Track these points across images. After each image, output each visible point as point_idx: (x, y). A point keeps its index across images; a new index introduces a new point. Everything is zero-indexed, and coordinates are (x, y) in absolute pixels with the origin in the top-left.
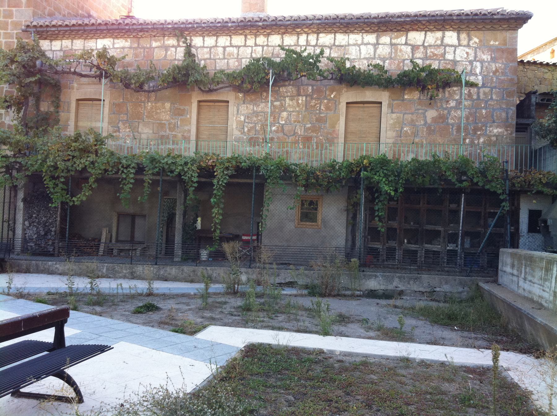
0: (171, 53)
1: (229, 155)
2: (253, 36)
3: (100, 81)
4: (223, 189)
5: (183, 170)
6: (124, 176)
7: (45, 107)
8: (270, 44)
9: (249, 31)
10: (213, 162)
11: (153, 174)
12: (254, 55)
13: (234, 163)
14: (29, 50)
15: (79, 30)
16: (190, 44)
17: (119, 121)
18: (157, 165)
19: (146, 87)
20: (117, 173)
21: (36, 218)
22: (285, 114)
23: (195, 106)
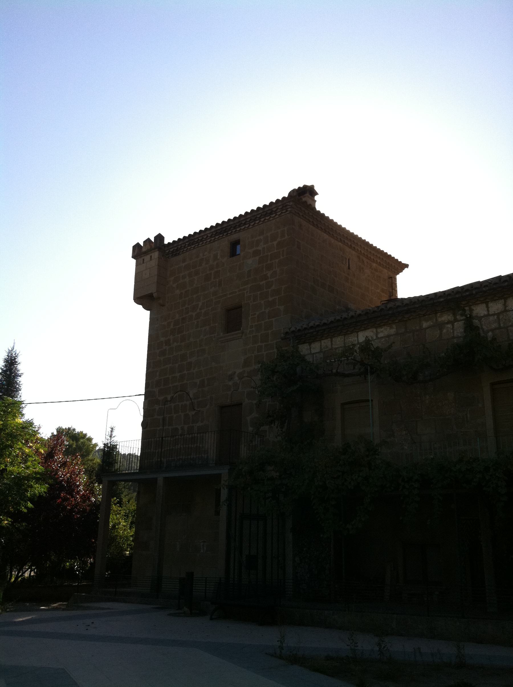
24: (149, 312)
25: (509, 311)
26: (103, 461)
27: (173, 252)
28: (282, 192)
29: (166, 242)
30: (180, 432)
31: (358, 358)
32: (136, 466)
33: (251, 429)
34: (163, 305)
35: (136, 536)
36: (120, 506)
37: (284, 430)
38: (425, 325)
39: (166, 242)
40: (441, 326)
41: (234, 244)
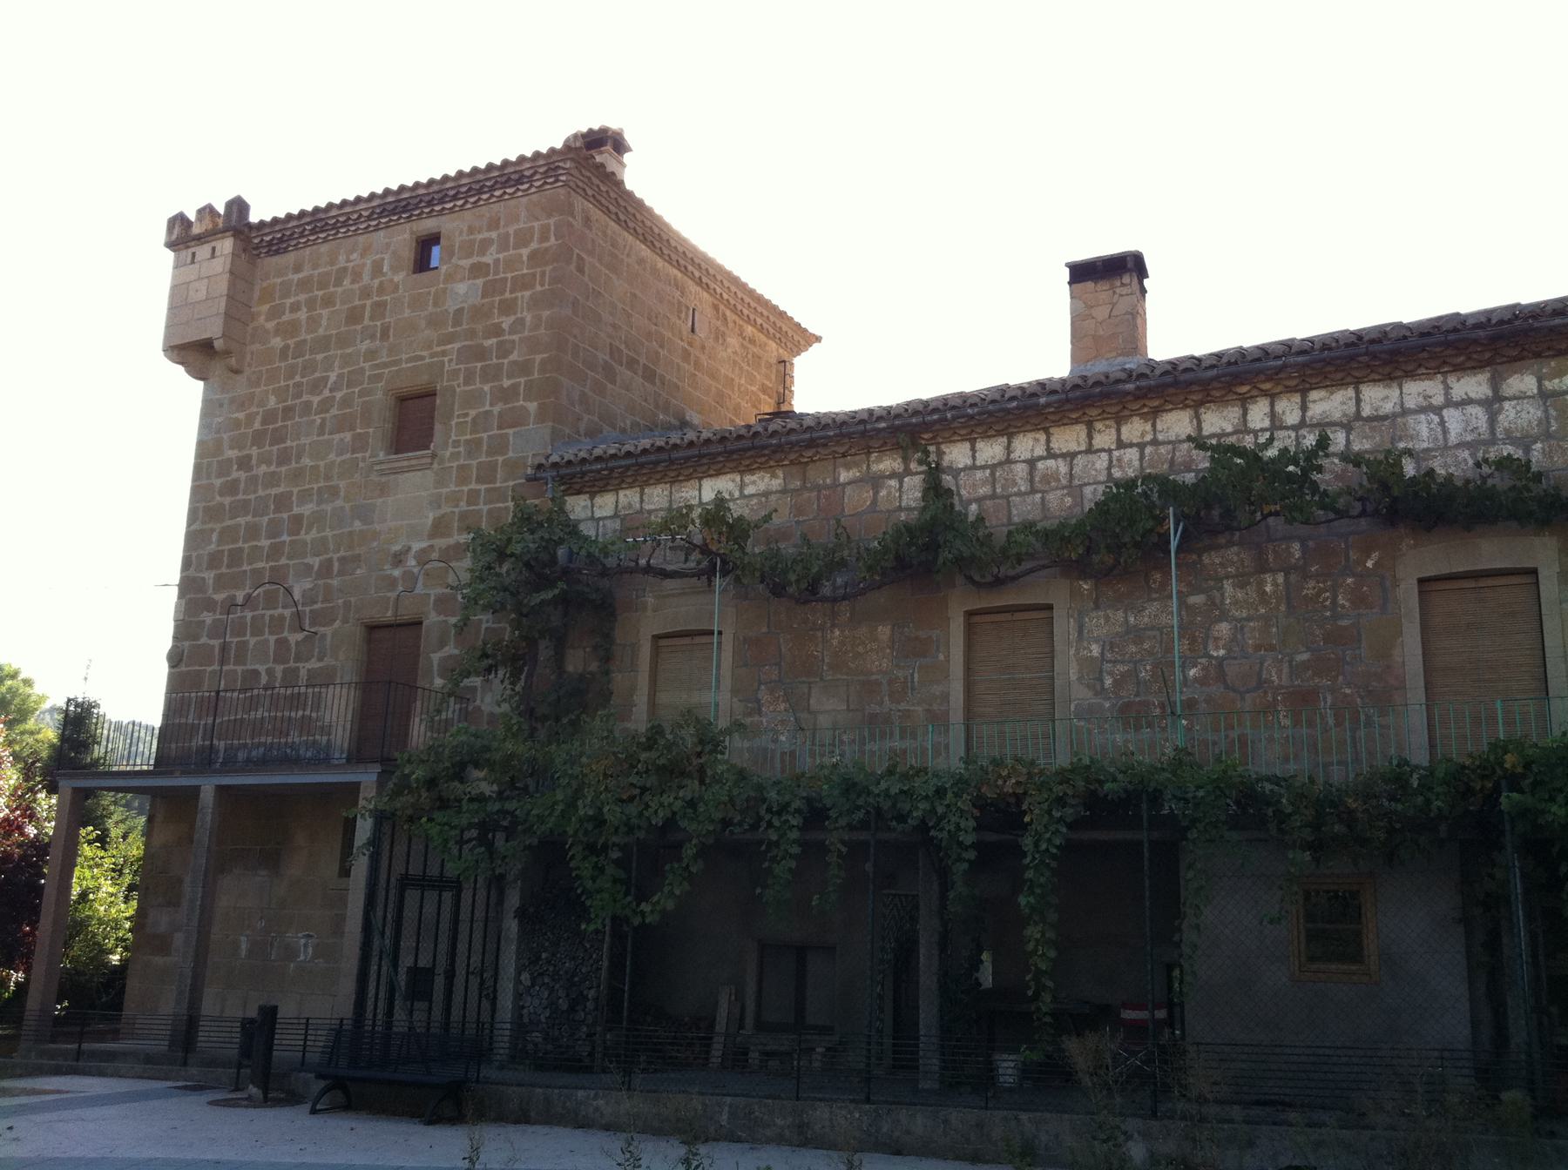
0: (889, 493)
1: (1063, 760)
2: (1111, 423)
4: (1054, 864)
5: (933, 811)
7: (576, 661)
8: (1160, 437)
10: (1018, 783)
11: (851, 827)
12: (1117, 473)
14: (540, 525)
18: (860, 802)
19: (826, 589)
21: (549, 962)
22: (1224, 628)
24: (201, 384)
26: (63, 738)
27: (270, 243)
28: (550, 136)
29: (254, 218)
30: (264, 679)
31: (697, 540)
32: (146, 754)
33: (439, 682)
34: (237, 372)
35: (139, 920)
36: (103, 848)
37: (518, 688)
38: (844, 476)
39: (254, 218)
40: (876, 481)
41: (426, 244)
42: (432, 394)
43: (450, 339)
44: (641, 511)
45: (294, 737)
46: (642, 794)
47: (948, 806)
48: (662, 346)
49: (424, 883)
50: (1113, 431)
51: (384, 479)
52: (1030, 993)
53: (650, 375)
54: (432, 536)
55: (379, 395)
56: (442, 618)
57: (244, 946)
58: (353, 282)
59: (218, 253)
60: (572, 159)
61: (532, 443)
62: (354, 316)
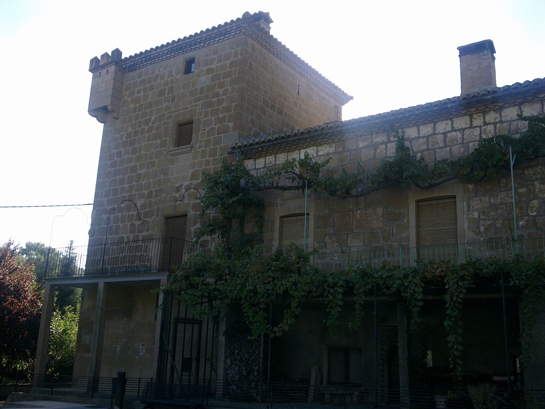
0: (381, 151)
1: (462, 260)
2: (481, 114)
3: (303, 193)
4: (460, 307)
5: (403, 284)
6: (331, 298)
7: (249, 228)
8: (503, 119)
9: (474, 110)
10: (442, 271)
11: (366, 293)
12: (484, 136)
13: (471, 270)
14: (233, 171)
15: (282, 143)
16: (402, 137)
17: (326, 235)
18: (369, 281)
19: (354, 192)
20: (322, 295)
21: (238, 355)
22: (535, 203)
23: (412, 207)
25: (438, 134)
27: (129, 67)
34: (116, 118)
41: (190, 63)
42: (191, 123)
43: (198, 100)
44: (275, 165)
45: (137, 263)
46: (273, 280)
47: (409, 282)
48: (285, 100)
49: (186, 321)
50: (482, 118)
51: (173, 157)
52: (451, 366)
53: (280, 112)
54: (191, 180)
55: (171, 124)
56: (195, 213)
57: (118, 349)
58: (161, 79)
59: (109, 72)
60: (246, 23)
61: (232, 139)
62: (161, 93)
